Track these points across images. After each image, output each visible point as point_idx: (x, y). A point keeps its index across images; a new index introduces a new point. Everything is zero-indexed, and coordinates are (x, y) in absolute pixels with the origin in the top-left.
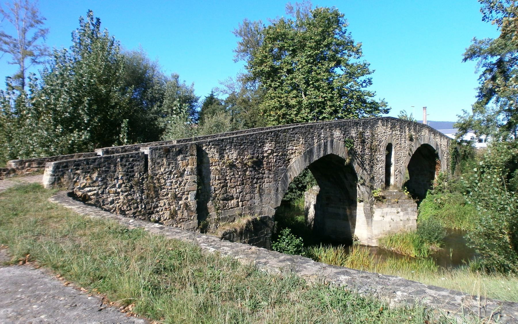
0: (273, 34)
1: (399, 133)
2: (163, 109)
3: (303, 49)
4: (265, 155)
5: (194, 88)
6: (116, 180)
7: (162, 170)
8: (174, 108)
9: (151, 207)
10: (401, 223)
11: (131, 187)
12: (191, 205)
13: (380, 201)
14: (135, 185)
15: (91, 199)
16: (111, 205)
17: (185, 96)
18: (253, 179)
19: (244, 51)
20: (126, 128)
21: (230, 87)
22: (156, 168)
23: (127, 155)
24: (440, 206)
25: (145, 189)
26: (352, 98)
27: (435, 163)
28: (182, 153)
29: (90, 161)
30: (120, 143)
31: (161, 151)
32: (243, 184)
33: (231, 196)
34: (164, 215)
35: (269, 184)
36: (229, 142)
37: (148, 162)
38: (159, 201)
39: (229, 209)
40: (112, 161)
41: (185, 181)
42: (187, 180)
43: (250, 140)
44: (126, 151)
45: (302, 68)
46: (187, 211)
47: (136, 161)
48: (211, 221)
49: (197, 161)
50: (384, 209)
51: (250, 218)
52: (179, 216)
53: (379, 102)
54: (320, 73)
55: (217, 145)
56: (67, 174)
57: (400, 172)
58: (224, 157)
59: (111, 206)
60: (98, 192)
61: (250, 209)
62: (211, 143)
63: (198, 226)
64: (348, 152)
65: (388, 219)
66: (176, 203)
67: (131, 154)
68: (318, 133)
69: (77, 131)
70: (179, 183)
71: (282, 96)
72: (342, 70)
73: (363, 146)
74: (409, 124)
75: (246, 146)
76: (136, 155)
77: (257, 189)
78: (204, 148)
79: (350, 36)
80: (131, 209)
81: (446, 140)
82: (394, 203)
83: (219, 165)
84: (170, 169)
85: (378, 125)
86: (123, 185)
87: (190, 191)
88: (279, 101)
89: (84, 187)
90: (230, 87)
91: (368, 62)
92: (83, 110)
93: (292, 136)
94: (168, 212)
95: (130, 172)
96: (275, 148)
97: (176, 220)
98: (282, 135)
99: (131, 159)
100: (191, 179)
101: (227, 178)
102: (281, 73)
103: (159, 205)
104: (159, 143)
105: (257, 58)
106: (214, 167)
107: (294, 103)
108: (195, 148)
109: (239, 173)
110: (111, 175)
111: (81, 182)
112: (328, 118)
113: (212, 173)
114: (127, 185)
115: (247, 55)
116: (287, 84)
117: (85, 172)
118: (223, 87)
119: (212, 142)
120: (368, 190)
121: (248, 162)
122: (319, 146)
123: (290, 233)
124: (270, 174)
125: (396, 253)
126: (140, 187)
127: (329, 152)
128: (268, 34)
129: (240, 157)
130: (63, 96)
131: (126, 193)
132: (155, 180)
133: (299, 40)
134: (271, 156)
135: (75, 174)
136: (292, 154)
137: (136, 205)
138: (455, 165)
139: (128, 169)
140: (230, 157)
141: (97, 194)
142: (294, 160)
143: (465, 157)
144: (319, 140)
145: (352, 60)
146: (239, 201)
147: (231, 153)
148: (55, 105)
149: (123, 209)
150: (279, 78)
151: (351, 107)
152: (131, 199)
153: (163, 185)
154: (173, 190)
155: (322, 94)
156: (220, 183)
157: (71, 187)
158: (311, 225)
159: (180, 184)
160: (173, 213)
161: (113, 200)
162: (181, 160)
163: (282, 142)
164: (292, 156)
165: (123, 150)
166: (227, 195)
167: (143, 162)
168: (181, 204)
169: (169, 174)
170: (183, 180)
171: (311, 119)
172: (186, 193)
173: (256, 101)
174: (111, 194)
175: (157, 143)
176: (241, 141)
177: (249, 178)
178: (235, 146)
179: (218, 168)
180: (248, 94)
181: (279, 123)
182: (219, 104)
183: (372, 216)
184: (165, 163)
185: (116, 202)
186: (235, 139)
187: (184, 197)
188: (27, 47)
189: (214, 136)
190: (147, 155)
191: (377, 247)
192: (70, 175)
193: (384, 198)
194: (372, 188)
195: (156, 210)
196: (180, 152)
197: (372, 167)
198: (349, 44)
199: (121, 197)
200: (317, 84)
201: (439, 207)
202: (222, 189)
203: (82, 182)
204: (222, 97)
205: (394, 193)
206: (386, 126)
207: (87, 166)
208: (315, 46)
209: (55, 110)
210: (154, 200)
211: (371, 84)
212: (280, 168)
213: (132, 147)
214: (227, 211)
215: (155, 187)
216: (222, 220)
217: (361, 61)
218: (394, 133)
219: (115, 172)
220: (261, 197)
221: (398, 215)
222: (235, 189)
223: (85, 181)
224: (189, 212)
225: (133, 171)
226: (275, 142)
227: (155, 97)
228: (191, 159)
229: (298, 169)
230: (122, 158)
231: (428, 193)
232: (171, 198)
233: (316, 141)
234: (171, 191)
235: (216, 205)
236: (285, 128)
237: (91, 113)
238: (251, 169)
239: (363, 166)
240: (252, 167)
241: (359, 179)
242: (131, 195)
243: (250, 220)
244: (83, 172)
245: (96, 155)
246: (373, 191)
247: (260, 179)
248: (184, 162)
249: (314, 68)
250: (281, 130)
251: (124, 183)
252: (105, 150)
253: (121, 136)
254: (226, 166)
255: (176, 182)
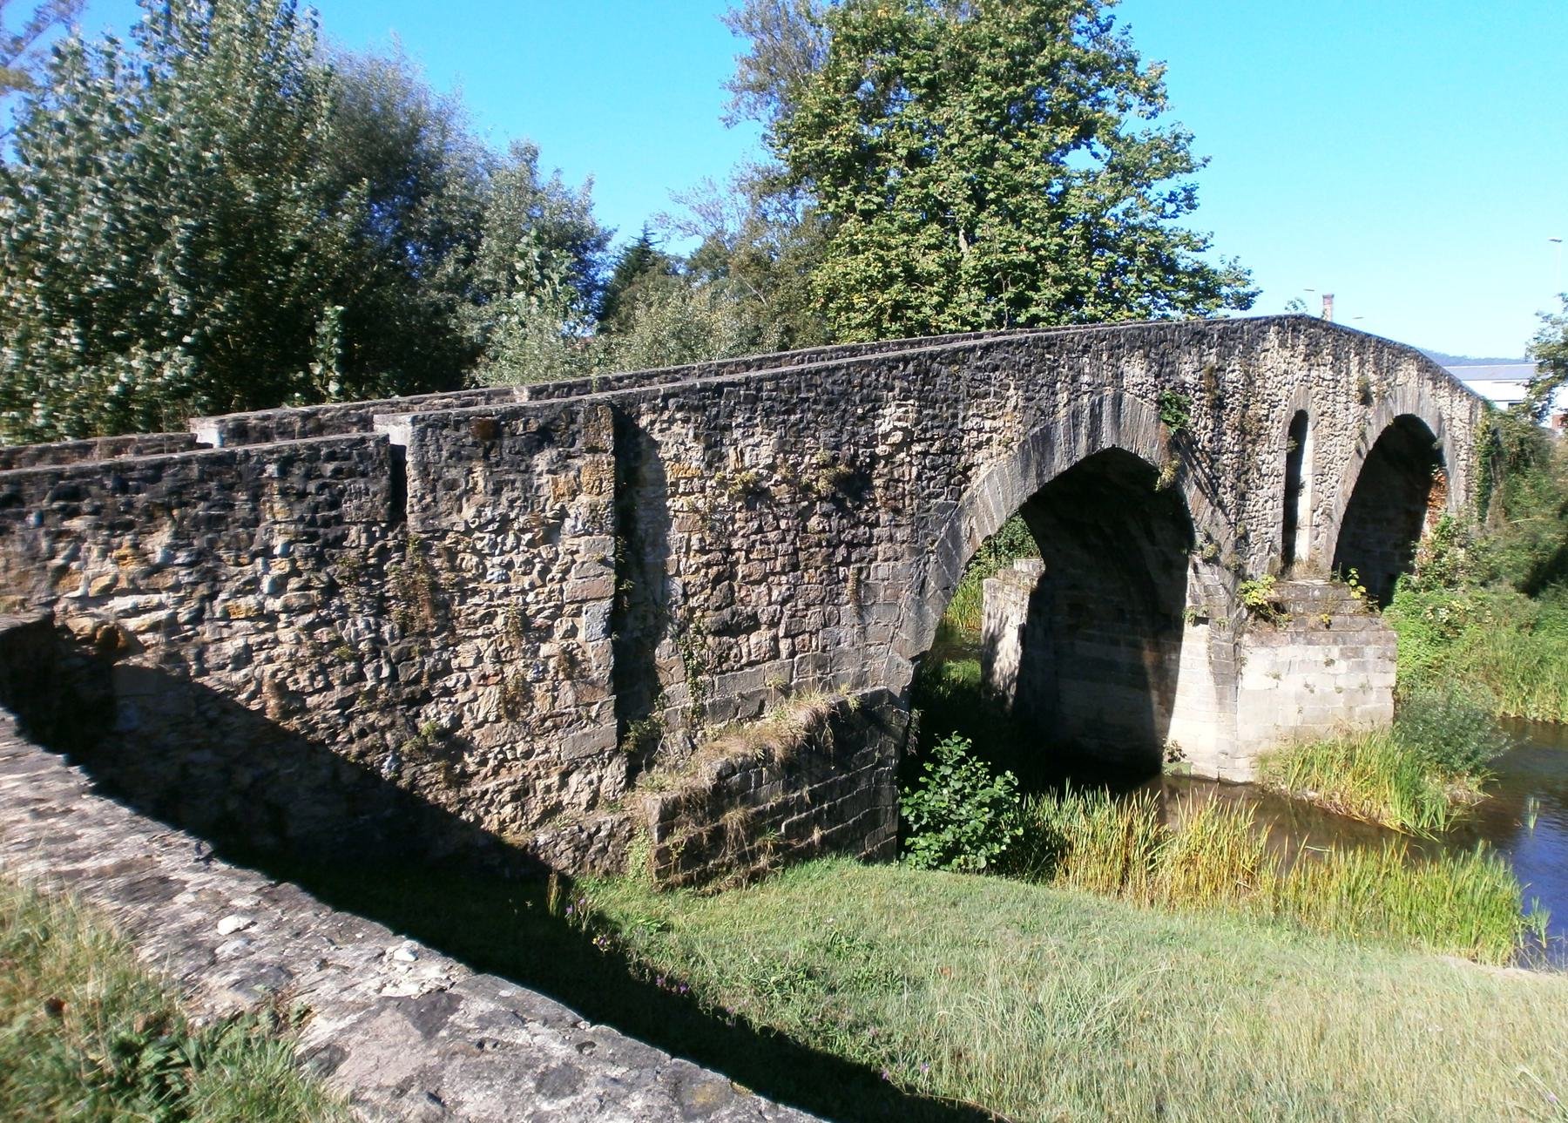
0: (865, 26)
1: (1329, 375)
2: (479, 273)
3: (966, 80)
4: (881, 450)
5: (594, 195)
6: (259, 561)
7: (468, 512)
8: (520, 266)
9: (421, 673)
10: (1340, 701)
11: (331, 589)
12: (589, 661)
13: (1266, 618)
14: (349, 579)
15: (141, 649)
16: (236, 669)
17: (562, 226)
18: (833, 545)
19: (760, 88)
20: (335, 341)
21: (708, 214)
22: (443, 507)
23: (310, 447)
24: (1448, 632)
25: (395, 597)
26: (1131, 253)
27: (1429, 483)
28: (552, 442)
29: (135, 474)
30: (315, 397)
31: (463, 432)
32: (795, 567)
33: (749, 617)
34: (475, 706)
35: (892, 563)
36: (746, 396)
37: (405, 478)
38: (455, 645)
39: (741, 668)
40: (240, 475)
41: (564, 559)
42: (573, 553)
43: (825, 392)
44: (320, 429)
45: (962, 144)
46: (573, 685)
47: (351, 474)
48: (671, 721)
49: (616, 475)
50: (1280, 651)
51: (820, 701)
52: (538, 704)
53: (1221, 268)
54: (1022, 166)
55: (696, 409)
56: (16, 537)
57: (1329, 516)
58: (722, 457)
59: (237, 677)
60: (174, 615)
61: (821, 665)
62: (671, 401)
63: (620, 743)
64: (1169, 443)
65: (1292, 684)
66: (525, 651)
67: (327, 443)
68: (1071, 369)
69: (144, 347)
70: (538, 567)
71: (893, 242)
72: (1096, 155)
73: (1218, 420)
74: (1362, 342)
75: (810, 415)
76: (350, 447)
77: (850, 585)
78: (644, 422)
79: (1125, 38)
80: (329, 686)
81: (1467, 403)
82: (1314, 629)
83: (703, 490)
84: (501, 510)
85: (1267, 345)
86: (294, 583)
87: (584, 601)
88: (881, 259)
89: (107, 593)
90: (708, 214)
91: (1185, 129)
92: (167, 265)
93: (979, 376)
94: (495, 691)
95: (327, 523)
96: (916, 425)
97: (526, 724)
98: (944, 371)
99: (329, 468)
100: (588, 550)
101: (735, 545)
102: (889, 161)
103: (454, 663)
104: (458, 397)
105: (805, 107)
106: (683, 500)
107: (934, 268)
108: (606, 420)
109: (783, 524)
110: (236, 536)
111: (89, 573)
112: (1046, 319)
113: (675, 523)
114: (309, 580)
115: (768, 103)
116: (908, 198)
117: (112, 527)
118: (682, 213)
119: (675, 395)
120: (1229, 578)
121: (817, 480)
122: (1075, 416)
123: (970, 753)
124: (897, 526)
125: (1326, 813)
126: (371, 588)
127: (1107, 441)
128: (846, 24)
129: (786, 460)
130: (86, 210)
131: (309, 618)
132: (438, 556)
133: (953, 49)
134: (902, 455)
135: (59, 535)
136: (979, 446)
137: (351, 666)
138: (1489, 488)
139: (315, 509)
140: (747, 458)
141: (171, 626)
142: (983, 471)
143: (1520, 463)
144: (1075, 394)
145: (1134, 124)
146: (781, 634)
147: (751, 441)
148: (55, 239)
149: (292, 688)
150: (881, 181)
151: (1123, 283)
152: (330, 642)
153: (475, 579)
154: (514, 597)
155: (1030, 237)
156: (708, 565)
157: (41, 596)
158: (1004, 698)
159: (545, 571)
160: (513, 697)
161: (247, 647)
162: (549, 472)
163: (946, 400)
164: (980, 456)
165: (311, 425)
166: (733, 614)
167: (384, 481)
168: (548, 657)
169: (497, 532)
170: (557, 554)
171: (989, 325)
172: (568, 609)
173: (797, 258)
174: (236, 624)
175: (450, 397)
176: (791, 392)
177: (819, 544)
178: (768, 413)
179: (700, 504)
180: (771, 237)
181: (881, 334)
182: (668, 271)
183: (1239, 672)
184: (481, 484)
185: (263, 655)
186: (768, 385)
187: (561, 626)
188: (9, 57)
189: (676, 372)
190: (400, 450)
191: (1250, 784)
192: (36, 538)
193: (1279, 607)
194: (1240, 574)
195: (439, 684)
196: (543, 438)
197: (1243, 496)
198: (1122, 67)
199: (286, 635)
200: (1012, 201)
201: (1442, 634)
202: (713, 589)
203: (97, 570)
204: (680, 247)
205: (1317, 593)
206: (1293, 347)
207: (121, 499)
208: (1009, 69)
209: (54, 265)
210: (435, 643)
211: (1192, 207)
212: (933, 501)
213: (346, 414)
214: (734, 677)
215: (435, 588)
216: (714, 713)
217: (1163, 125)
218: (1314, 373)
219: (256, 522)
220: (861, 617)
221: (1330, 669)
222: (763, 588)
223: (109, 566)
224: (581, 687)
225: (339, 520)
226: (919, 399)
227: (450, 228)
228: (591, 468)
229: (997, 504)
230: (286, 464)
231: (1399, 585)
232: (508, 633)
233: (1063, 397)
234: (505, 601)
235: (691, 655)
236: (956, 345)
237: (195, 276)
238: (827, 507)
239: (1216, 492)
240: (833, 498)
241: (1199, 539)
242: (329, 623)
243: (823, 709)
244: (98, 527)
245: (192, 443)
246: (1243, 586)
247: (859, 545)
248: (562, 478)
249: (1003, 146)
250: (943, 352)
251: (295, 572)
252: (231, 425)
253: (317, 370)
254: (731, 496)
255: (529, 563)
